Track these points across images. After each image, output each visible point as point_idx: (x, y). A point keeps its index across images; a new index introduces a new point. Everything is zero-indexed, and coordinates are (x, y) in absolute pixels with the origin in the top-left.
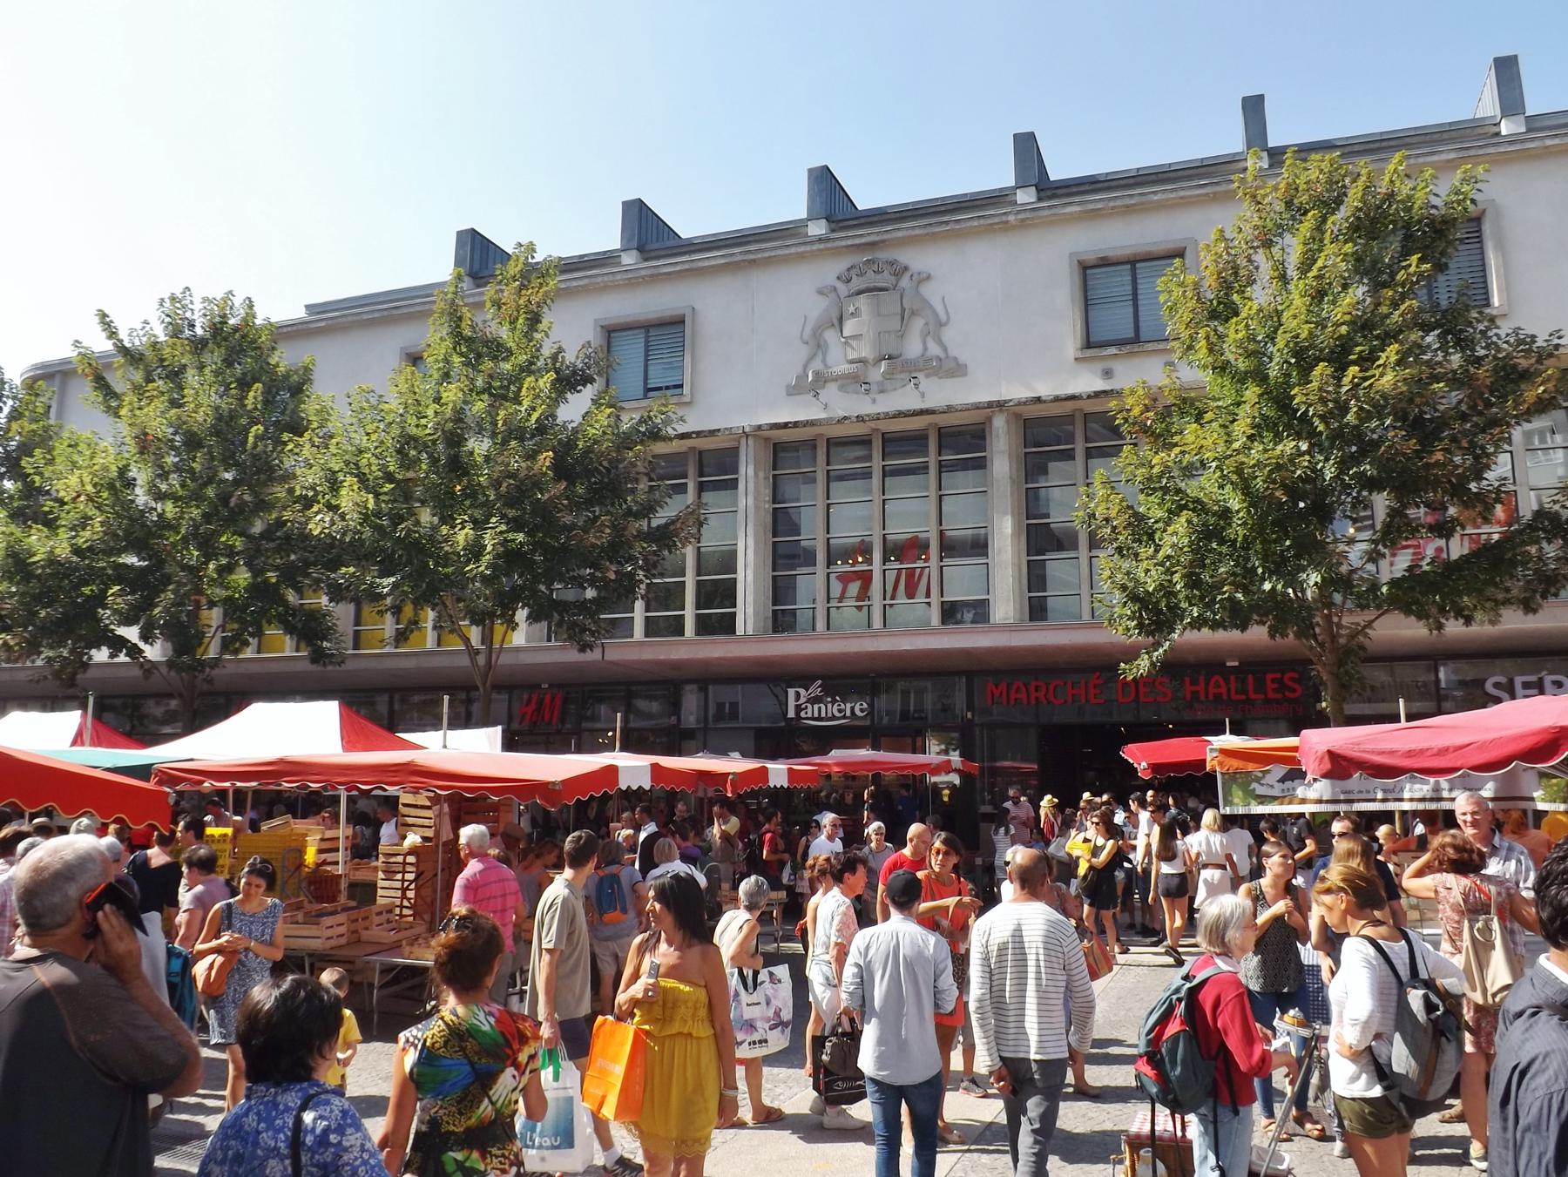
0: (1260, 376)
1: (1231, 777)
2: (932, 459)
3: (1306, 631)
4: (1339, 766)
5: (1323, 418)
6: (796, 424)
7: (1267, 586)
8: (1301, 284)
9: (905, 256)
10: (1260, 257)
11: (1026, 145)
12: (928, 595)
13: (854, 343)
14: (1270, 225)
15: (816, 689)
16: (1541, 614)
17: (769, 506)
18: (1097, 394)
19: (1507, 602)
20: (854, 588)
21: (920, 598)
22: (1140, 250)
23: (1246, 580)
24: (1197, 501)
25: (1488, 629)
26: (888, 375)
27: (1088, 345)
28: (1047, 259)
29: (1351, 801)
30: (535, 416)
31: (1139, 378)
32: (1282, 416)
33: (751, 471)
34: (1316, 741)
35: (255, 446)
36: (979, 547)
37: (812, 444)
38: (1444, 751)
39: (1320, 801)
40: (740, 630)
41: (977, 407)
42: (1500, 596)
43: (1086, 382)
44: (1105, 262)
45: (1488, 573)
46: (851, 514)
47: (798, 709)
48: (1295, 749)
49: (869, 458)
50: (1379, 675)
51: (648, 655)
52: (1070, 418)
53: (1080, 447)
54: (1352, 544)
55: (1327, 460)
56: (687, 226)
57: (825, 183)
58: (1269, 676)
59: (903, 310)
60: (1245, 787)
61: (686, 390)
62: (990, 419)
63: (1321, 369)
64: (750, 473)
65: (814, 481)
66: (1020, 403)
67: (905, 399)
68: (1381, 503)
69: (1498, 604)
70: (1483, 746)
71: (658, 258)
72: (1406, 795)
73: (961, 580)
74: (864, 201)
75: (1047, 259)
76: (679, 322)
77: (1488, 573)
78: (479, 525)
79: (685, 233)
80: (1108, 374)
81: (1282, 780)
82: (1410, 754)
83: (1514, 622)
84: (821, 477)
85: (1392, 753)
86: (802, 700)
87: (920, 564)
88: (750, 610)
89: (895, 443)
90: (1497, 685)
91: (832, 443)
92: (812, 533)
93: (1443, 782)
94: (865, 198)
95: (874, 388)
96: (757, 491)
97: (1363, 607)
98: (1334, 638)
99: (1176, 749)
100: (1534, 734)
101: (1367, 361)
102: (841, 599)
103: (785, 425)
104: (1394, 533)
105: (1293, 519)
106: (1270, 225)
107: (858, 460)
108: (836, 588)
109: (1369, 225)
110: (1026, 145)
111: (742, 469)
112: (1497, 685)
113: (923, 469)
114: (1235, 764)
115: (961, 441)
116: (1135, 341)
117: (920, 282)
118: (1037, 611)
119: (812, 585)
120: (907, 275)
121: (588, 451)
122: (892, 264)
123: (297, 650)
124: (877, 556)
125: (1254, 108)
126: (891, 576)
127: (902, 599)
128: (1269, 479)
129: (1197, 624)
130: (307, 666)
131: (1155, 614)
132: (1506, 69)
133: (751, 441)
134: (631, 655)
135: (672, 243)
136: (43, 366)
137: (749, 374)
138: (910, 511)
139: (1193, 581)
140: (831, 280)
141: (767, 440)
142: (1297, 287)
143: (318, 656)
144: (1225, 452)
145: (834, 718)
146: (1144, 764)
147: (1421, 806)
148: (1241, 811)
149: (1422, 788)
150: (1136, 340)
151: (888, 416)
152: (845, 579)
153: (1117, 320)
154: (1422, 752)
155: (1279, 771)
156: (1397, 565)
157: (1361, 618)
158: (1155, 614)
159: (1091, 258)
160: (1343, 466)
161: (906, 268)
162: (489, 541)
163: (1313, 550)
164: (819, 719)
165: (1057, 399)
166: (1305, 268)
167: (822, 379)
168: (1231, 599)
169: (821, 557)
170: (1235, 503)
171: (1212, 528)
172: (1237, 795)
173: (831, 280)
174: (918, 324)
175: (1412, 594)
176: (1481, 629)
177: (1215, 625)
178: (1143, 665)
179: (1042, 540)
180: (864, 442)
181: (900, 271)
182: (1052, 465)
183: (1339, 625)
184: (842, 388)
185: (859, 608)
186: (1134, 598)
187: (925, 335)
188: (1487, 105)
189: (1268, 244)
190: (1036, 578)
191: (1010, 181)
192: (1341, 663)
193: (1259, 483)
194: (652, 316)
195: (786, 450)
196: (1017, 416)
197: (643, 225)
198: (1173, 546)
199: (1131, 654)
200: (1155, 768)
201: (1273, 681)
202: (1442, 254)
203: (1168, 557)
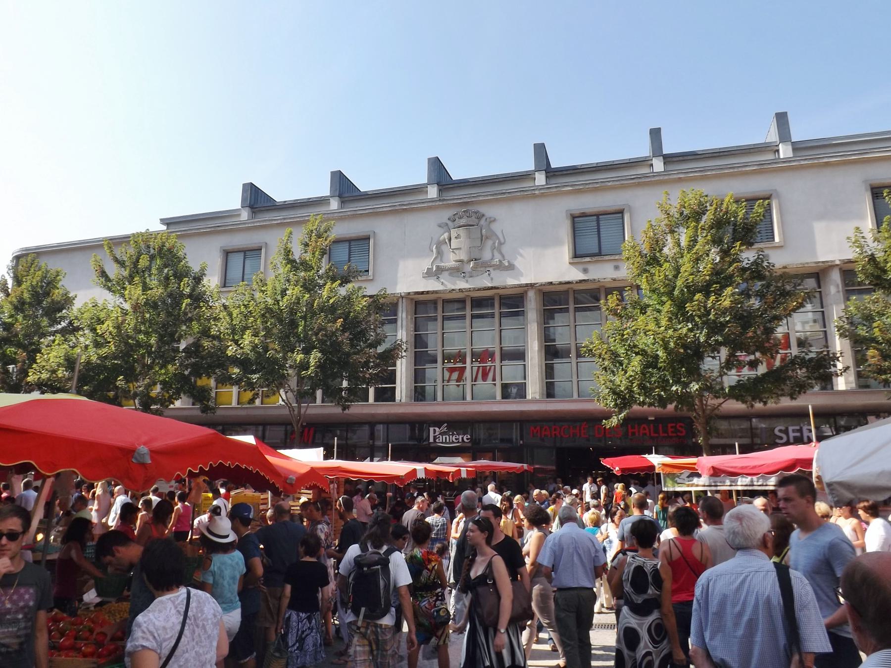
0: (670, 294)
1: (667, 475)
2: (496, 311)
3: (691, 407)
4: (716, 472)
5: (699, 317)
6: (428, 292)
7: (674, 388)
8: (688, 256)
9: (483, 209)
10: (669, 237)
11: (540, 151)
12: (494, 380)
13: (456, 251)
14: (673, 223)
15: (444, 428)
16: (798, 399)
17: (413, 333)
18: (581, 281)
19: (783, 395)
20: (455, 375)
21: (489, 381)
22: (602, 209)
23: (664, 384)
24: (643, 350)
25: (774, 405)
26: (474, 269)
27: (576, 255)
28: (555, 213)
29: (716, 486)
30: (331, 301)
31: (603, 272)
32: (680, 311)
33: (404, 315)
34: (706, 461)
35: (186, 308)
36: (519, 355)
37: (435, 302)
38: (754, 467)
39: (704, 486)
40: (398, 397)
41: (520, 286)
42: (780, 393)
43: (574, 275)
44: (584, 215)
45: (776, 381)
46: (457, 336)
47: (435, 438)
48: (695, 464)
49: (464, 308)
50: (723, 425)
51: (372, 411)
52: (566, 292)
53: (572, 306)
54: (710, 364)
55: (701, 333)
56: (363, 186)
57: (436, 166)
58: (669, 425)
59: (482, 236)
60: (673, 479)
61: (371, 273)
62: (526, 292)
63: (698, 296)
64: (403, 315)
65: (436, 320)
66: (541, 285)
67: (484, 281)
68: (724, 352)
69: (778, 396)
70: (769, 465)
71: (356, 204)
72: (739, 483)
73: (510, 372)
74: (455, 177)
75: (555, 213)
76: (367, 238)
77: (776, 381)
78: (307, 351)
79: (363, 188)
80: (585, 271)
81: (688, 477)
82: (742, 468)
83: (786, 402)
84: (440, 319)
85: (735, 467)
86: (437, 433)
87: (489, 364)
88: (404, 386)
89: (478, 303)
90: (780, 431)
91: (446, 302)
92: (434, 346)
93: (755, 478)
94: (456, 174)
95: (467, 275)
96: (407, 325)
97: (717, 397)
98: (704, 411)
99: (631, 461)
100: (780, 463)
101: (719, 293)
102: (448, 381)
103: (422, 293)
104: (729, 364)
105: (687, 359)
106: (673, 223)
107: (458, 310)
108: (447, 374)
109: (719, 224)
110: (540, 151)
111: (400, 314)
112: (780, 431)
113: (492, 316)
114: (669, 470)
115: (512, 302)
116: (598, 254)
117: (490, 222)
118: (550, 392)
119: (435, 373)
120: (484, 219)
121: (356, 317)
122: (476, 213)
123: (193, 404)
124: (468, 360)
125: (655, 134)
126: (475, 369)
127: (480, 381)
128: (675, 343)
129: (643, 404)
130: (198, 413)
131: (624, 400)
132: (782, 119)
133: (404, 300)
134: (366, 411)
135: (356, 194)
136: (27, 249)
137: (406, 269)
138: (486, 336)
139: (642, 386)
140: (445, 220)
141: (412, 299)
142: (687, 257)
143: (205, 409)
144: (653, 330)
145: (453, 442)
146: (617, 468)
147: (746, 488)
148: (671, 489)
149: (747, 480)
150: (599, 254)
151: (475, 290)
152: (452, 370)
153: (589, 243)
154: (746, 467)
155: (687, 472)
156: (731, 379)
157: (716, 402)
158: (624, 400)
159: (577, 212)
160: (708, 336)
161: (483, 215)
162: (312, 362)
163: (695, 373)
164: (446, 443)
165: (561, 283)
166: (690, 248)
167: (440, 270)
168: (659, 395)
169: (440, 359)
170: (660, 353)
171: (651, 362)
172: (669, 482)
173: (445, 220)
174: (489, 243)
175: (740, 391)
176: (772, 405)
177: (650, 405)
178: (614, 421)
179: (552, 352)
180: (462, 301)
181: (480, 216)
182: (556, 315)
183: (706, 405)
184: (450, 274)
185: (458, 386)
186: (614, 393)
187: (493, 248)
188: (772, 136)
189: (672, 232)
190: (549, 371)
191: (532, 167)
192: (707, 423)
193: (672, 345)
194: (353, 235)
195: (423, 305)
196: (540, 290)
197: (342, 184)
198: (633, 371)
199: (608, 417)
200: (622, 470)
201: (672, 427)
202: (751, 238)
203: (631, 376)
